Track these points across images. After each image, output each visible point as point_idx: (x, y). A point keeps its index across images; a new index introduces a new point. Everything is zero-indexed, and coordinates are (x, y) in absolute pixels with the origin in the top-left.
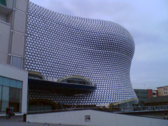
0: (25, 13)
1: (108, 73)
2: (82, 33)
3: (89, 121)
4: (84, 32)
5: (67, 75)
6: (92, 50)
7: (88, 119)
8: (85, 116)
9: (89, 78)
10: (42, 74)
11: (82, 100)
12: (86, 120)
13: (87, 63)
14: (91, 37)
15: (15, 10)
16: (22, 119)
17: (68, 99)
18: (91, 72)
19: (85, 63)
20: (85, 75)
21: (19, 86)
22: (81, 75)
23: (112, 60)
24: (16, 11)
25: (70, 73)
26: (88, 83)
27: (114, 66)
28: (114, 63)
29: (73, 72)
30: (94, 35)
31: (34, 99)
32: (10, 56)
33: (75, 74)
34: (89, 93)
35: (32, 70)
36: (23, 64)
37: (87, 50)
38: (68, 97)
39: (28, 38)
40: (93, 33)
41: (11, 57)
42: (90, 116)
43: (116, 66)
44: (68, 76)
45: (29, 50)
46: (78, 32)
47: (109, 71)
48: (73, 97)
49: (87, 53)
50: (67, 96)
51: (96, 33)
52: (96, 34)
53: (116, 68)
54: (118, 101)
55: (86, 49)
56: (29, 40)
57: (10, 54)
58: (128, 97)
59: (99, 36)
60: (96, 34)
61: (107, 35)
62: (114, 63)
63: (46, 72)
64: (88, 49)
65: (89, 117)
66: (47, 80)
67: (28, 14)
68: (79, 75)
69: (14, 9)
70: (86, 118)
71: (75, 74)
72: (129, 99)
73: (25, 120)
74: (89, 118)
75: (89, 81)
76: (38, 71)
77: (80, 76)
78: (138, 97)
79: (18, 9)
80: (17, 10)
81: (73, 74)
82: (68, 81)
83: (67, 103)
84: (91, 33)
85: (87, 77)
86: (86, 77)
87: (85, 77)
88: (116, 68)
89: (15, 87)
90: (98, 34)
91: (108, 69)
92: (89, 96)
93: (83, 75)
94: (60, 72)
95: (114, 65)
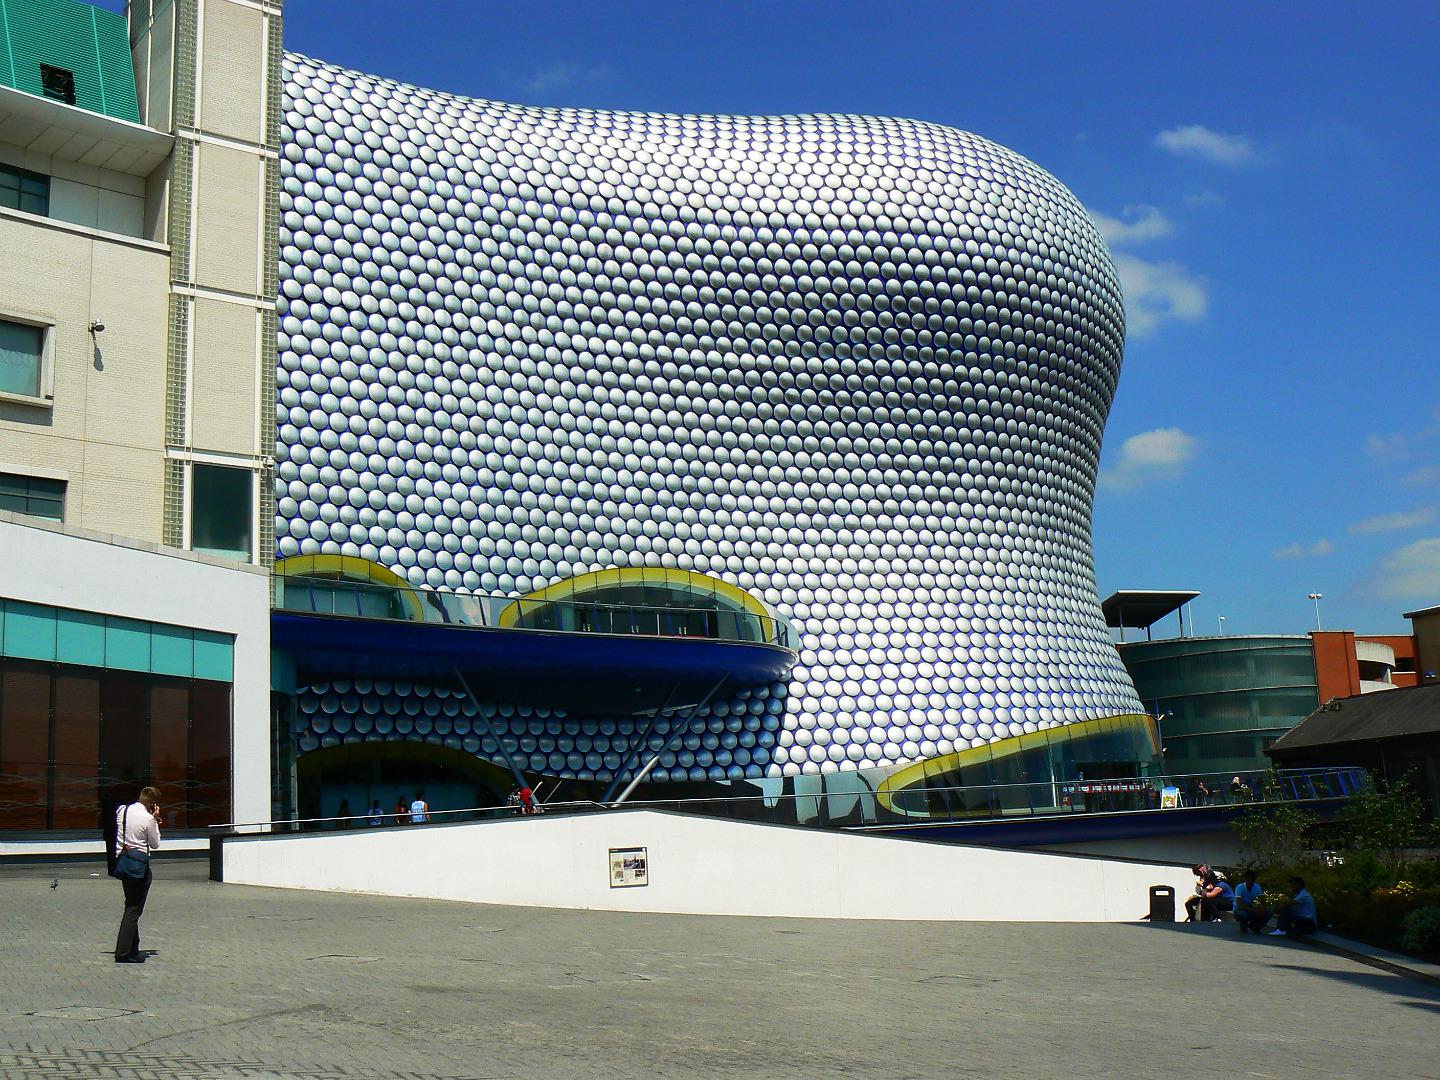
0: (263, 152)
1: (893, 535)
2: (712, 242)
3: (642, 880)
4: (693, 228)
5: (578, 567)
6: (763, 359)
7: (630, 873)
8: (611, 851)
9: (745, 578)
10: (396, 569)
11: (677, 743)
12: (619, 875)
13: (727, 467)
14: (746, 261)
15: (191, 141)
16: (204, 868)
17: (584, 745)
18: (762, 531)
19: (711, 466)
20: (716, 561)
21: (203, 665)
22: (683, 559)
23: (903, 427)
24: (196, 149)
25: (602, 553)
26: (740, 619)
27: (938, 475)
28: (938, 455)
29: (625, 539)
30: (774, 247)
31: (350, 745)
32: (175, 461)
33: (634, 556)
34: (766, 693)
35: (328, 546)
36: (219, 507)
37: (727, 368)
38: (591, 730)
39: (290, 322)
40: (765, 233)
41: (181, 469)
42: (640, 849)
43: (952, 476)
44: (590, 570)
45: (297, 413)
46: (649, 238)
47: (900, 520)
48: (586, 727)
49: (726, 388)
50: (581, 718)
51: (787, 226)
52: (783, 233)
53: (953, 486)
54: (960, 744)
55: (714, 355)
56: (299, 341)
57: (175, 454)
58: (1043, 712)
59: (810, 248)
60: (783, 233)
61: (873, 235)
62: (938, 455)
63: (424, 554)
64: (730, 357)
65: (641, 856)
66: (360, 613)
67: (275, 155)
68: (667, 558)
69: (182, 133)
70: (618, 864)
71: (634, 556)
72: (1054, 725)
73: (216, 874)
74: (640, 865)
75: (750, 609)
76: (367, 550)
77: (678, 567)
78: (1149, 706)
79: (205, 133)
80: (203, 138)
81: (618, 555)
82: (589, 606)
83: (502, 752)
84: (746, 232)
85: (728, 577)
86: (721, 573)
87: (711, 574)
88: (953, 486)
89: (49, 658)
90: (802, 234)
91: (890, 504)
92: (746, 717)
93: (700, 560)
94: (520, 546)
95: (940, 468)
